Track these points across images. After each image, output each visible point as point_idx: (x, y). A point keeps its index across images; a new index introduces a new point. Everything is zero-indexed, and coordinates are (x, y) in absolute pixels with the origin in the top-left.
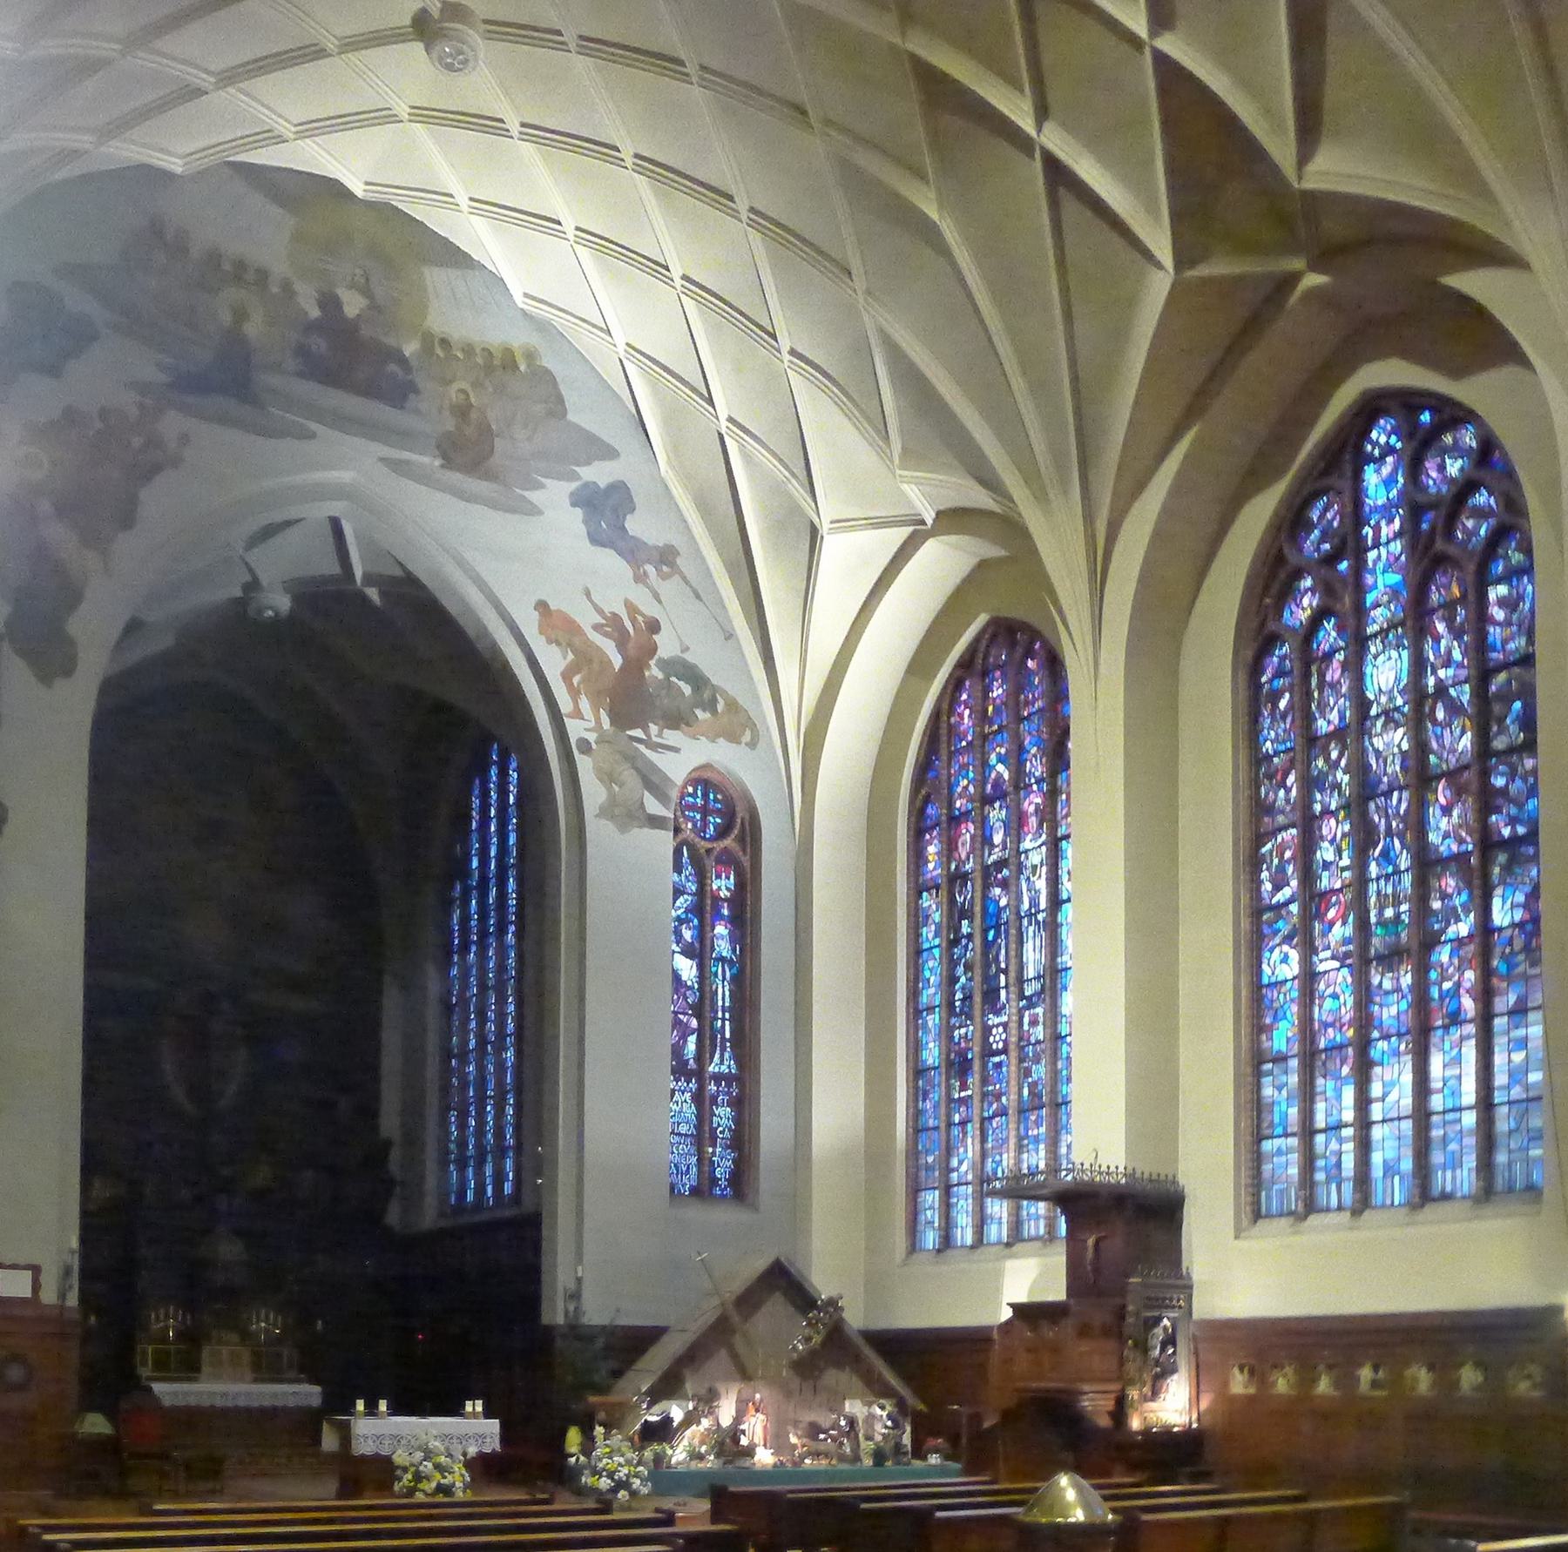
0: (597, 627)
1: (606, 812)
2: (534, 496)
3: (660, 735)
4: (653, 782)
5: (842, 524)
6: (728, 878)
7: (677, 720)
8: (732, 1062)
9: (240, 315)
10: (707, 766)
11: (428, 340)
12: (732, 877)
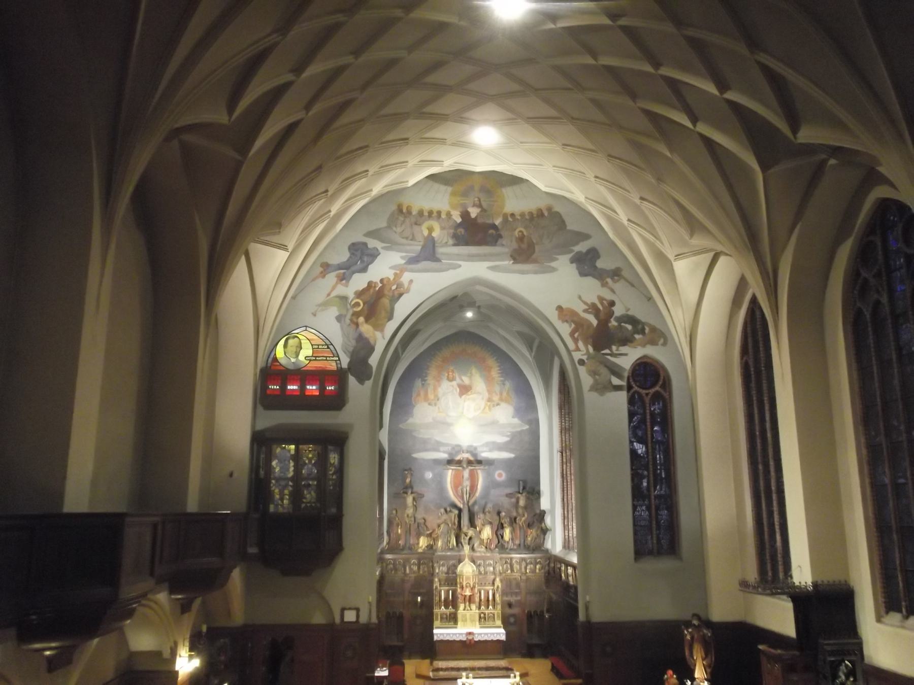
0: (585, 311)
1: (594, 388)
2: (553, 264)
3: (617, 350)
4: (615, 371)
5: (678, 256)
6: (659, 404)
7: (626, 341)
8: (667, 489)
9: (431, 230)
10: (645, 357)
11: (505, 216)
12: (661, 403)
